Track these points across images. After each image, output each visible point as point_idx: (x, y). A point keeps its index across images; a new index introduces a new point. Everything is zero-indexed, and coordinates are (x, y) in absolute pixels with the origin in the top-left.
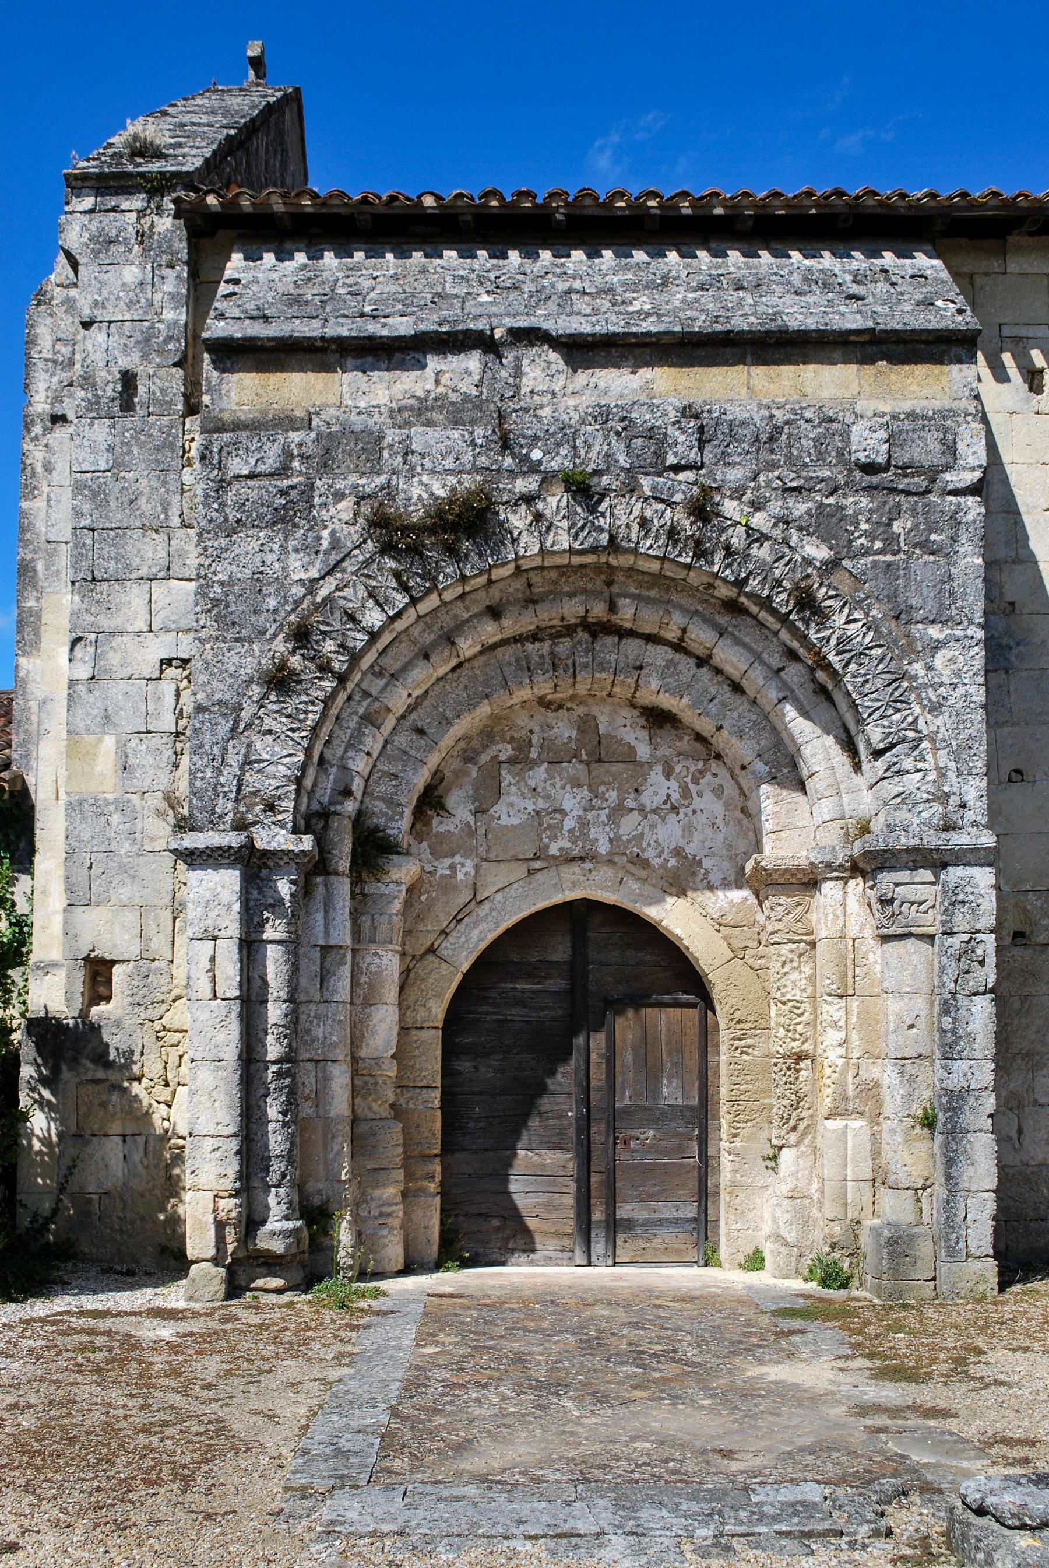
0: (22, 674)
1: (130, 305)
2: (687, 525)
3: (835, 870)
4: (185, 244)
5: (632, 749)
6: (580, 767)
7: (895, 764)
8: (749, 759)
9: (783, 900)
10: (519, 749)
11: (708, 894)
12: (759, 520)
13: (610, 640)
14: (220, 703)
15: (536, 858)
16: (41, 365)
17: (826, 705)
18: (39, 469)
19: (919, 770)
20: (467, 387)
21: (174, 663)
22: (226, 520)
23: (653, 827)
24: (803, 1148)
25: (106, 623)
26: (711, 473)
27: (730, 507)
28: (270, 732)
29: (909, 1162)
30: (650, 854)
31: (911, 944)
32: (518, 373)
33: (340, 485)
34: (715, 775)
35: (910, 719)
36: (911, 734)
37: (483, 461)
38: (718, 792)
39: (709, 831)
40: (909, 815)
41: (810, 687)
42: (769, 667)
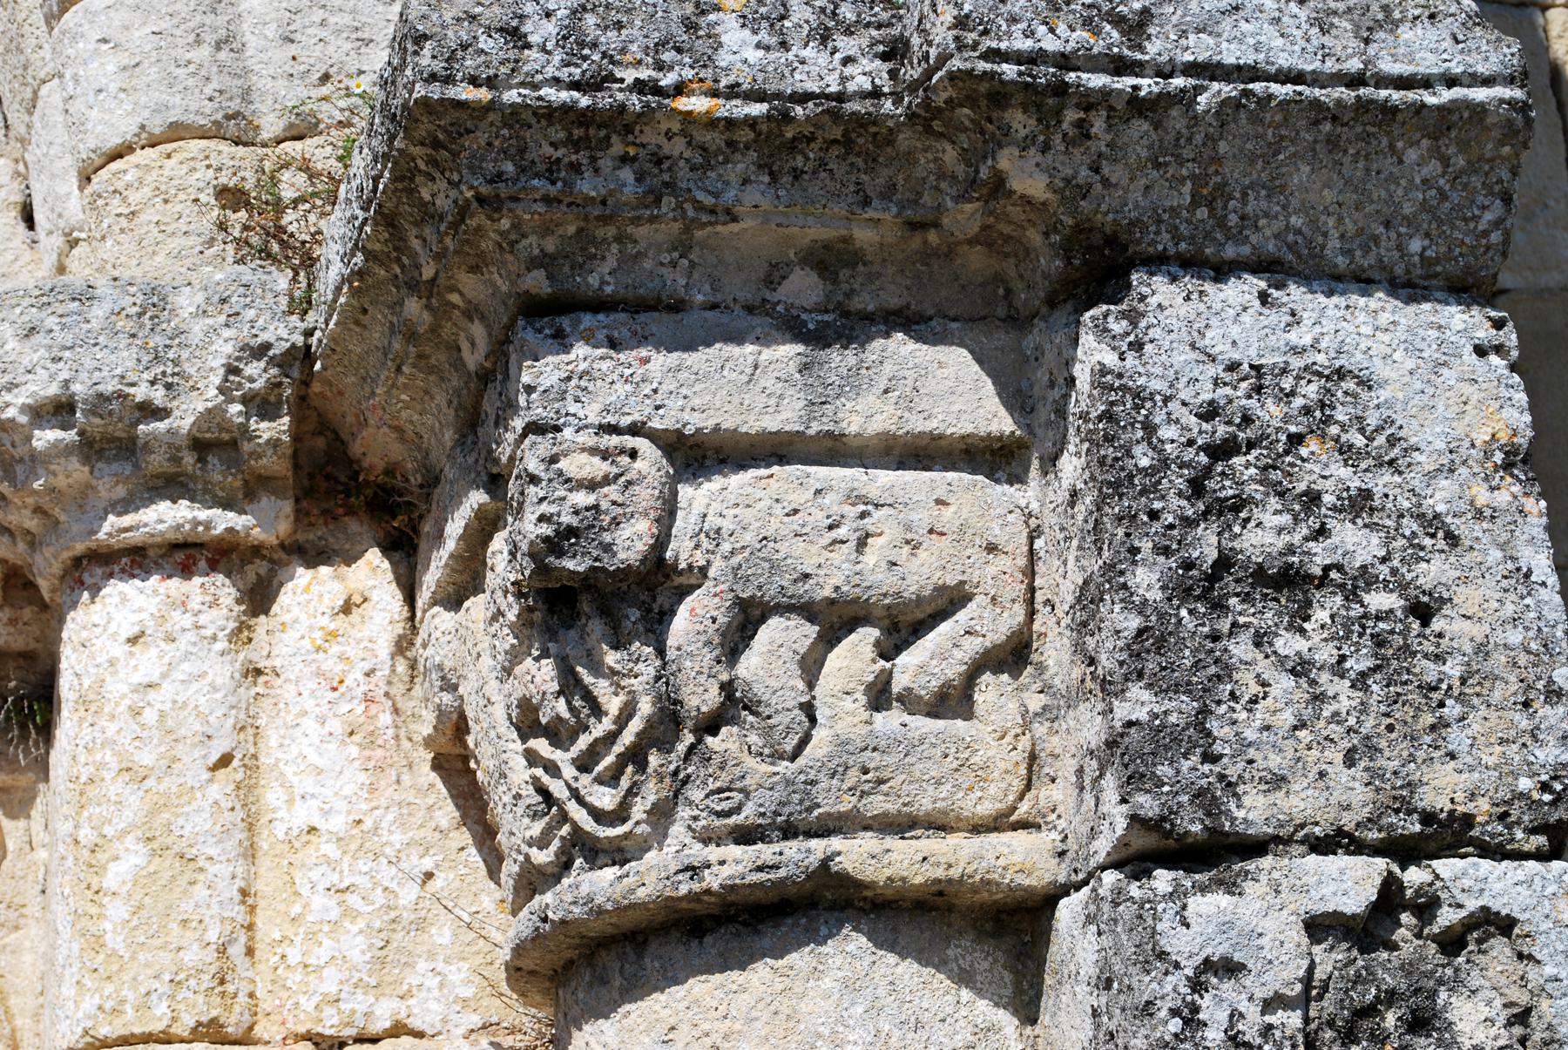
3: (171, 486)
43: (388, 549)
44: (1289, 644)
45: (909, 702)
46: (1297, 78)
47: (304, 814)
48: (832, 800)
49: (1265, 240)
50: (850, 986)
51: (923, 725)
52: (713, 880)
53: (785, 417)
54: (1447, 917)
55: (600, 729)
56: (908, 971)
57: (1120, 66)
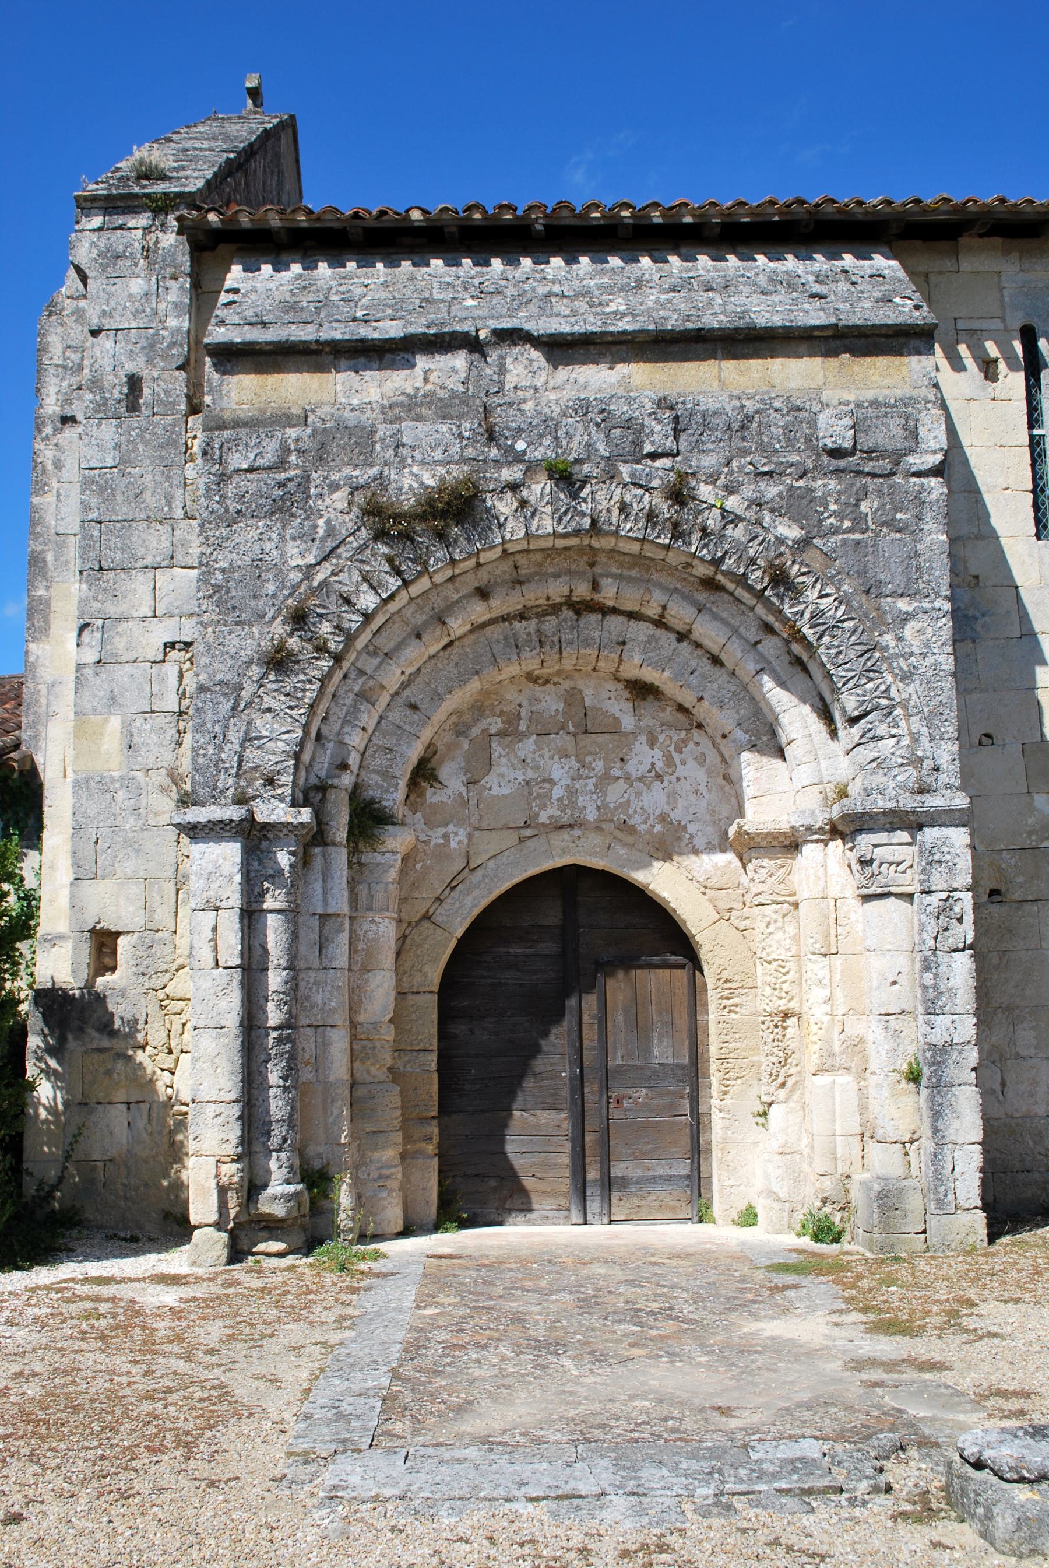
0: (31, 659)
1: (136, 314)
2: (665, 509)
3: (816, 833)
4: (187, 258)
5: (617, 721)
6: (569, 738)
7: (870, 730)
8: (730, 728)
9: (766, 862)
10: (508, 722)
11: (693, 858)
12: (733, 503)
13: (594, 618)
14: (221, 683)
15: (527, 825)
16: (52, 370)
17: (802, 675)
18: (50, 467)
20: (454, 384)
21: (177, 646)
22: (227, 511)
23: (638, 794)
24: (791, 1104)
25: (112, 609)
26: (686, 459)
27: (705, 491)
28: (269, 710)
30: (636, 820)
32: (502, 370)
33: (335, 477)
34: (697, 744)
35: (883, 688)
36: (884, 702)
37: (470, 452)
38: (701, 760)
39: (693, 798)
40: (885, 779)
41: (786, 658)
42: (746, 640)
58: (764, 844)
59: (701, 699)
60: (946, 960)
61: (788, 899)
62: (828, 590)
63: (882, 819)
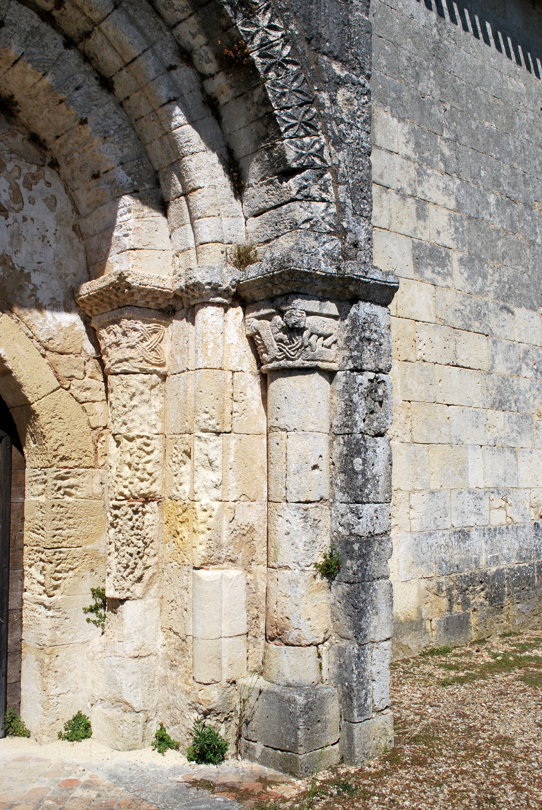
3: (219, 295)
7: (305, 187)
8: (110, 165)
9: (139, 325)
11: (36, 313)
17: (211, 120)
19: (323, 200)
24: (149, 600)
29: (313, 615)
31: (316, 379)
34: (49, 184)
35: (317, 146)
39: (38, 244)
40: (315, 243)
41: (198, 95)
42: (161, 60)
43: (242, 306)
44: (369, 347)
45: (325, 346)
46: (379, 281)
47: (231, 342)
48: (317, 357)
49: (371, 298)
50: (316, 379)
51: (327, 349)
52: (305, 365)
53: (317, 310)
54: (379, 380)
55: (293, 345)
56: (321, 378)
57: (364, 277)
58: (141, 303)
59: (84, 122)
60: (372, 444)
61: (158, 369)
62: (276, 23)
63: (319, 283)
